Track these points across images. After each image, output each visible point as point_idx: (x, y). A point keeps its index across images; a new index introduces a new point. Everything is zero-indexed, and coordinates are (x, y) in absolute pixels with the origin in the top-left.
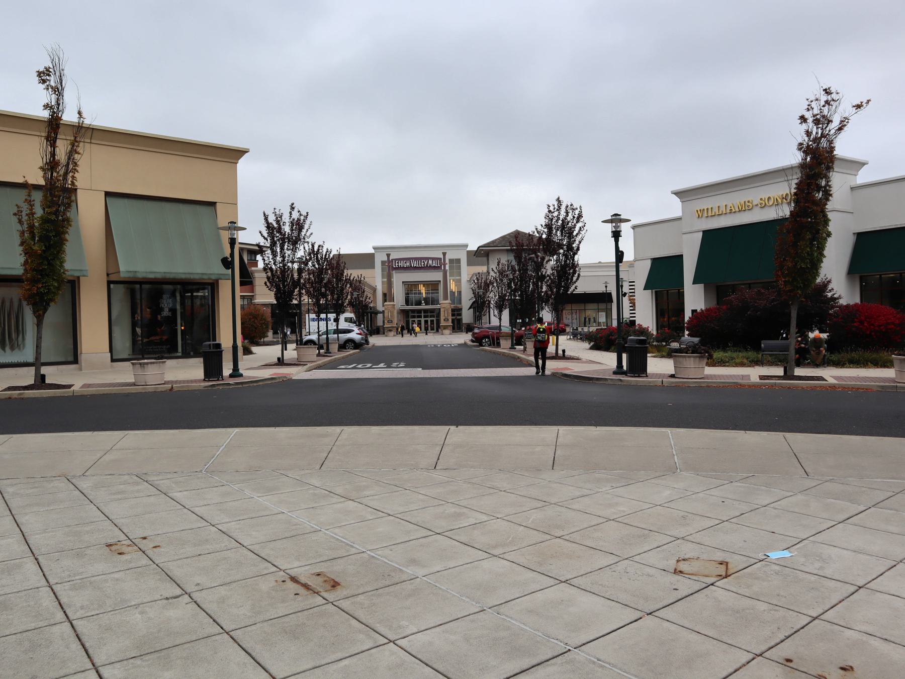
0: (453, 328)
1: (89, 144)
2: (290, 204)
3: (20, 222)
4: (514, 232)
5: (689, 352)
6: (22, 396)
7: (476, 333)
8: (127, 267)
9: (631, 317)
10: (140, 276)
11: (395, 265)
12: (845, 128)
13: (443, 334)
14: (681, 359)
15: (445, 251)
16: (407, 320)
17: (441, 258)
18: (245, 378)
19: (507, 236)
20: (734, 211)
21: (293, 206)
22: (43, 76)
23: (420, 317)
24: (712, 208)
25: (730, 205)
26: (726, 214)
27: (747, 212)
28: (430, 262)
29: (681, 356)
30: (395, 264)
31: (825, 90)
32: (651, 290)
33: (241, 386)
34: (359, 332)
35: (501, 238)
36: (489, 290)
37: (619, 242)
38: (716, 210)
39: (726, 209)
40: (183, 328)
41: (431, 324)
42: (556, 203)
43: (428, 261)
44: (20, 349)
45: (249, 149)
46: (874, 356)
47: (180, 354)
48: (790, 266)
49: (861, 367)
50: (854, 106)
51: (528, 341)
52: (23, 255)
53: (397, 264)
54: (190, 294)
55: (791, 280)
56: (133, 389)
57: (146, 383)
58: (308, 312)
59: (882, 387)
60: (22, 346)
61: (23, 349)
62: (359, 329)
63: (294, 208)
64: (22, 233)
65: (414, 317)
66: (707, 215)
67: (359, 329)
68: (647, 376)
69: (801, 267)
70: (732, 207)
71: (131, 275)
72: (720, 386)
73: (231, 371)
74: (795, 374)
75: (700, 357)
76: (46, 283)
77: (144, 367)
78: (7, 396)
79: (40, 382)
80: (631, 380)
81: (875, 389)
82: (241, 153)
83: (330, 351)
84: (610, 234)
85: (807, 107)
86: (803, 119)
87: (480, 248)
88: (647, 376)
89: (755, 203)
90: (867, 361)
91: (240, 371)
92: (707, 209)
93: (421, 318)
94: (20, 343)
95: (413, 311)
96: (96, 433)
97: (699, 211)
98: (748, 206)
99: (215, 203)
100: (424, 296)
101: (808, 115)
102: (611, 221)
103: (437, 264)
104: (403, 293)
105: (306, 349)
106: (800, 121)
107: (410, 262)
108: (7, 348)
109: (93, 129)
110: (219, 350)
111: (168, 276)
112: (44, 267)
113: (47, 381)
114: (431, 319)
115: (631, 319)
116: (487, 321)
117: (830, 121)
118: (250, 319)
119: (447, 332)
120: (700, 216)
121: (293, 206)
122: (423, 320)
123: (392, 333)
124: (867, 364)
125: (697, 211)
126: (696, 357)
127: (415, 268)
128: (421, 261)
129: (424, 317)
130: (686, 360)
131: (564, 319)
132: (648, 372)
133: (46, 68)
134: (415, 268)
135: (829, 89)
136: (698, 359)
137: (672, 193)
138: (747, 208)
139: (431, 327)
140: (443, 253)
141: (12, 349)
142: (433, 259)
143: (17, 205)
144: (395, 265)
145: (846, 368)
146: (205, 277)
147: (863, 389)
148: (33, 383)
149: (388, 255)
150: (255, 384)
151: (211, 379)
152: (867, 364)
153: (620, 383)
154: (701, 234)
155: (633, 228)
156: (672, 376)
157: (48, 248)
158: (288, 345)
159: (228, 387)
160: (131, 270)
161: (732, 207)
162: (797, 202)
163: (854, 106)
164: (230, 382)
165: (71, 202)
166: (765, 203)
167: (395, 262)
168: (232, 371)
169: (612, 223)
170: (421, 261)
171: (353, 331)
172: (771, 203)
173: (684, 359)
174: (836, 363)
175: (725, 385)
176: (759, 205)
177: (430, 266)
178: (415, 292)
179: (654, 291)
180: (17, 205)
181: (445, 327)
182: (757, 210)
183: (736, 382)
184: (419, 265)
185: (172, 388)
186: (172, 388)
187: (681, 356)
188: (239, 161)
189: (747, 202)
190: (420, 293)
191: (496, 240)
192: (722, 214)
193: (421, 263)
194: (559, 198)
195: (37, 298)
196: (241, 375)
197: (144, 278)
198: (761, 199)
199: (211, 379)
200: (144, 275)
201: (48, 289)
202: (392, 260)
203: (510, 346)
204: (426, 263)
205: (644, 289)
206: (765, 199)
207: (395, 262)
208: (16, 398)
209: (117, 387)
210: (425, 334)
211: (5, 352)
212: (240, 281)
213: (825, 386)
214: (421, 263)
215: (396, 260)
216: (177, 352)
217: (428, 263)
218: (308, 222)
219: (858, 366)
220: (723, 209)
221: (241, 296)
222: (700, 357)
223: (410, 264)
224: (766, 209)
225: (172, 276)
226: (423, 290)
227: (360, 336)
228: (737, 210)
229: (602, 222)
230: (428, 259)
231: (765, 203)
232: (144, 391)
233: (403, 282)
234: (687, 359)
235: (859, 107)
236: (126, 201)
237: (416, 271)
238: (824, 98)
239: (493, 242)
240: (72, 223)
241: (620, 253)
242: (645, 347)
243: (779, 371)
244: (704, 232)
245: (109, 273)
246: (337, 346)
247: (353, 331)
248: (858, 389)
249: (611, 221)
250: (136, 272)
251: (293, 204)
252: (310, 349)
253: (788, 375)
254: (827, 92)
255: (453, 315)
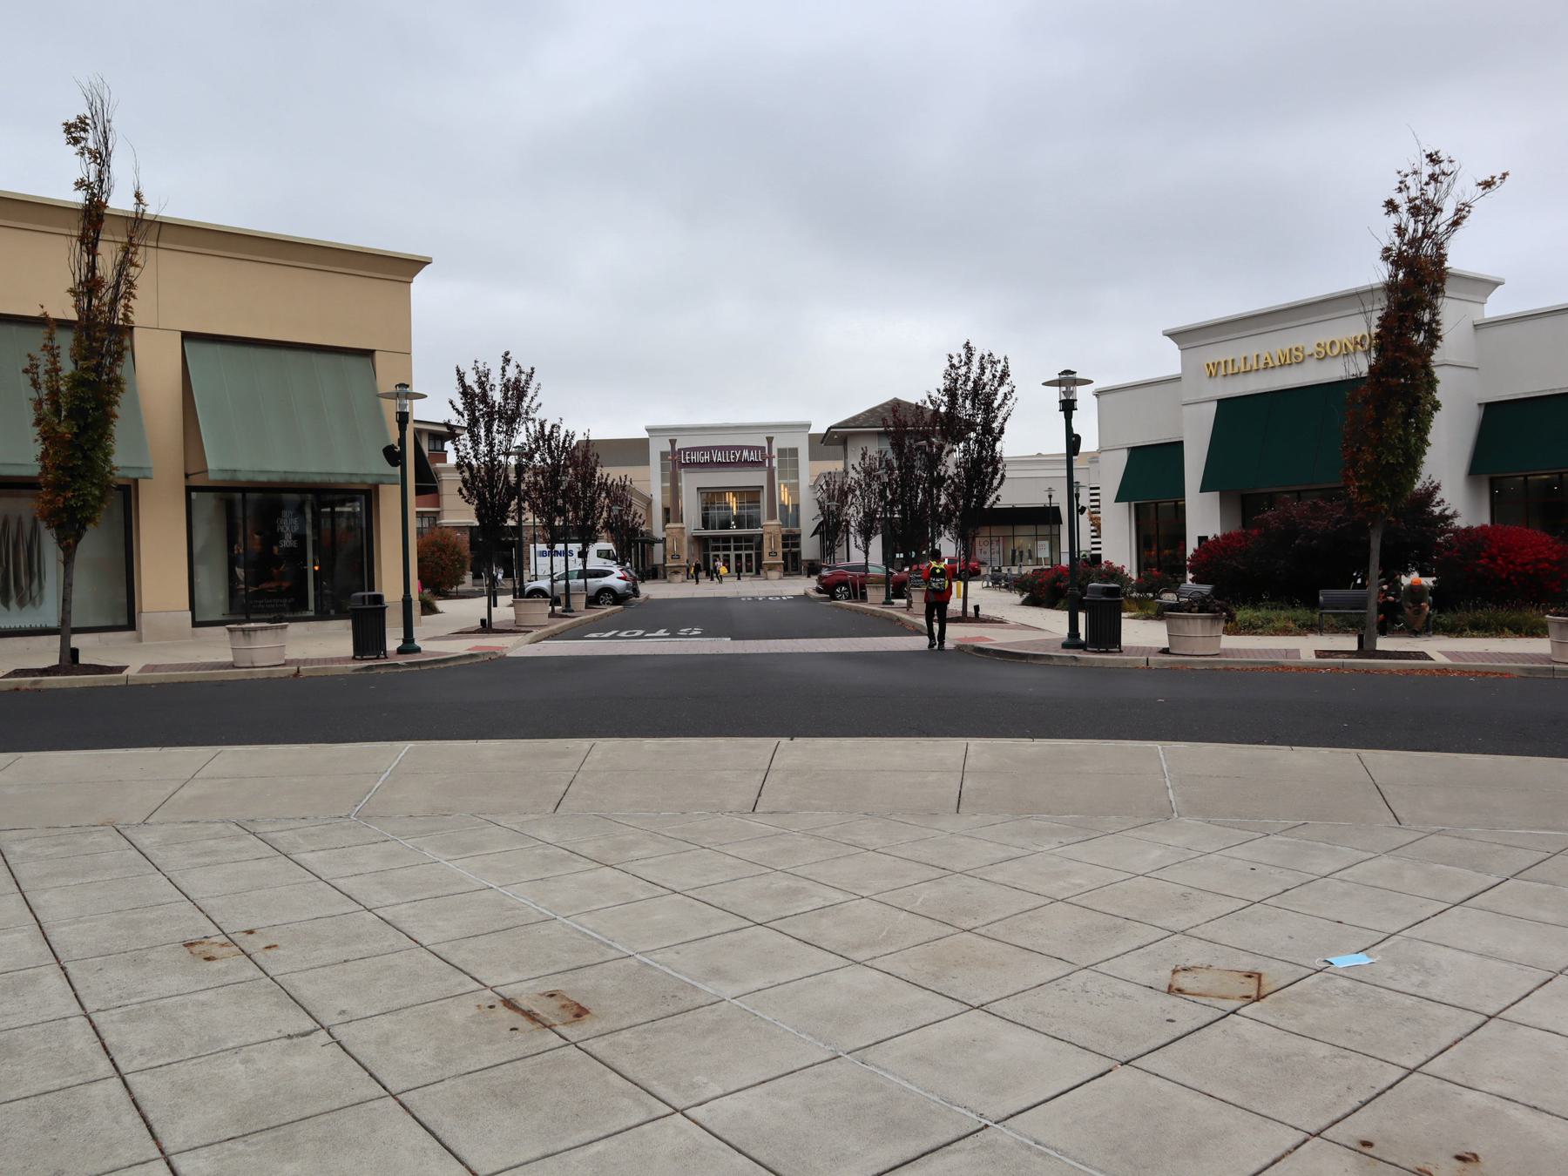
0: (784, 568)
1: (155, 250)
2: (503, 354)
3: (35, 384)
4: (891, 401)
5: (1193, 610)
6: (38, 687)
7: (825, 577)
8: (220, 462)
9: (1093, 549)
10: (242, 477)
11: (685, 460)
12: (1465, 222)
13: (767, 579)
14: (1180, 622)
15: (771, 435)
16: (704, 555)
17: (764, 448)
18: (424, 655)
19: (878, 409)
20: (1271, 365)
21: (508, 357)
22: (75, 131)
23: (728, 549)
24: (1233, 361)
25: (1264, 354)
26: (1257, 370)
27: (1294, 368)
28: (746, 453)
29: (1180, 617)
30: (685, 457)
31: (1430, 156)
32: (1127, 503)
33: (417, 669)
34: (622, 575)
35: (868, 411)
36: (847, 503)
37: (1073, 420)
38: (1240, 364)
39: (1257, 361)
40: (317, 568)
41: (747, 561)
42: (963, 352)
43: (742, 452)
44: (34, 604)
45: (431, 258)
46: (1515, 616)
47: (312, 614)
48: (1368, 460)
49: (1492, 636)
50: (1480, 184)
51: (914, 591)
52: (40, 442)
53: (687, 458)
54: (328, 510)
55: (1370, 484)
56: (230, 674)
57: (252, 663)
58: (534, 540)
59: (1529, 670)
60: (37, 599)
61: (41, 604)
62: (621, 570)
63: (509, 361)
64: (39, 403)
65: (717, 549)
66: (1226, 372)
67: (621, 570)
68: (1121, 651)
69: (1388, 462)
70: (1269, 358)
71: (227, 476)
72: (1247, 669)
73: (400, 643)
74: (1377, 648)
75: (1213, 619)
76: (79, 489)
77: (249, 635)
78: (12, 687)
79: (70, 662)
80: (1093, 658)
81: (1516, 673)
82: (418, 264)
83: (572, 607)
84: (1058, 406)
85: (1399, 185)
86: (1391, 206)
87: (832, 430)
88: (1121, 651)
89: (1308, 352)
90: (1502, 625)
91: (416, 643)
92: (1226, 362)
93: (730, 550)
94: (34, 594)
95: (716, 539)
96: (166, 750)
97: (1211, 366)
98: (1296, 357)
99: (373, 351)
100: (735, 513)
101: (1400, 199)
102: (1058, 383)
103: (758, 458)
104: (698, 507)
105: (530, 604)
106: (1385, 210)
107: (711, 453)
108: (13, 603)
109: (161, 223)
110: (379, 606)
111: (291, 478)
112: (75, 462)
113: (82, 660)
114: (747, 552)
115: (1093, 552)
116: (843, 556)
117: (1437, 210)
118: (433, 553)
119: (774, 574)
120: (1213, 374)
121: (508, 357)
122: (732, 554)
123: (679, 577)
124: (1503, 631)
125: (1208, 365)
126: (1207, 618)
127: (720, 464)
128: (729, 453)
129: (735, 550)
130: (1188, 624)
131: (977, 553)
132: (1123, 644)
133: (79, 118)
134: (720, 464)
135: (1436, 154)
136: (1209, 621)
137: (1165, 335)
138: (1294, 360)
139: (746, 566)
140: (767, 438)
141: (21, 604)
142: (750, 448)
143: (29, 356)
144: (685, 460)
145: (1466, 637)
146: (356, 480)
147: (1495, 674)
148: (57, 663)
149: (673, 442)
150: (442, 666)
151: (365, 657)
152: (1503, 631)
153: (1074, 664)
154: (1215, 405)
155: (1096, 395)
156: (1165, 651)
157: (83, 429)
158: (498, 598)
159: (396, 670)
160: (228, 468)
161: (1269, 358)
162: (1380, 349)
163: (1480, 184)
164: (399, 662)
165: (123, 350)
166: (1326, 352)
167: (685, 454)
168: (402, 643)
169: (1060, 386)
170: (729, 453)
171: (612, 573)
172: (1336, 351)
173: (1186, 622)
174: (1449, 629)
175: (1255, 666)
176: (1316, 356)
177: (746, 461)
178: (719, 505)
179: (1133, 503)
180: (29, 356)
181: (772, 567)
182: (1311, 365)
183: (1274, 662)
184: (725, 459)
185: (298, 671)
186: (298, 671)
187: (1180, 617)
188: (415, 278)
189: (1294, 351)
190: (728, 508)
191: (859, 416)
192: (1250, 371)
193: (729, 456)
194: (968, 343)
195: (65, 515)
196: (418, 650)
197: (249, 482)
198: (1319, 345)
199: (365, 657)
200: (250, 477)
201: (83, 500)
202: (680, 450)
203: (884, 600)
204: (738, 456)
205: (1116, 501)
206: (1325, 344)
207: (685, 454)
208: (27, 690)
209: (203, 670)
210: (736, 578)
211: (8, 609)
212: (416, 486)
213: (1429, 669)
214: (729, 456)
215: (685, 450)
216: (307, 609)
217: (741, 456)
218: (533, 385)
219: (1487, 634)
220: (1252, 362)
221: (417, 512)
222: (1212, 619)
223: (711, 457)
224: (1327, 361)
225: (297, 478)
226: (732, 501)
227: (624, 582)
228: (1277, 363)
229: (1043, 384)
230: (741, 448)
231: (1326, 352)
232: (249, 678)
233: (698, 488)
234: (1191, 621)
235: (1487, 185)
236: (218, 348)
237: (721, 469)
238: (1427, 169)
239: (854, 419)
240: (125, 387)
241: (1074, 439)
242: (1117, 601)
243: (1350, 643)
244: (1219, 401)
245: (189, 473)
246: (583, 599)
247: (612, 573)
248: (1487, 673)
249: (1058, 383)
250: (235, 471)
251: (507, 353)
252: (538, 604)
253: (1365, 650)
254: (1433, 159)
255: (785, 546)
